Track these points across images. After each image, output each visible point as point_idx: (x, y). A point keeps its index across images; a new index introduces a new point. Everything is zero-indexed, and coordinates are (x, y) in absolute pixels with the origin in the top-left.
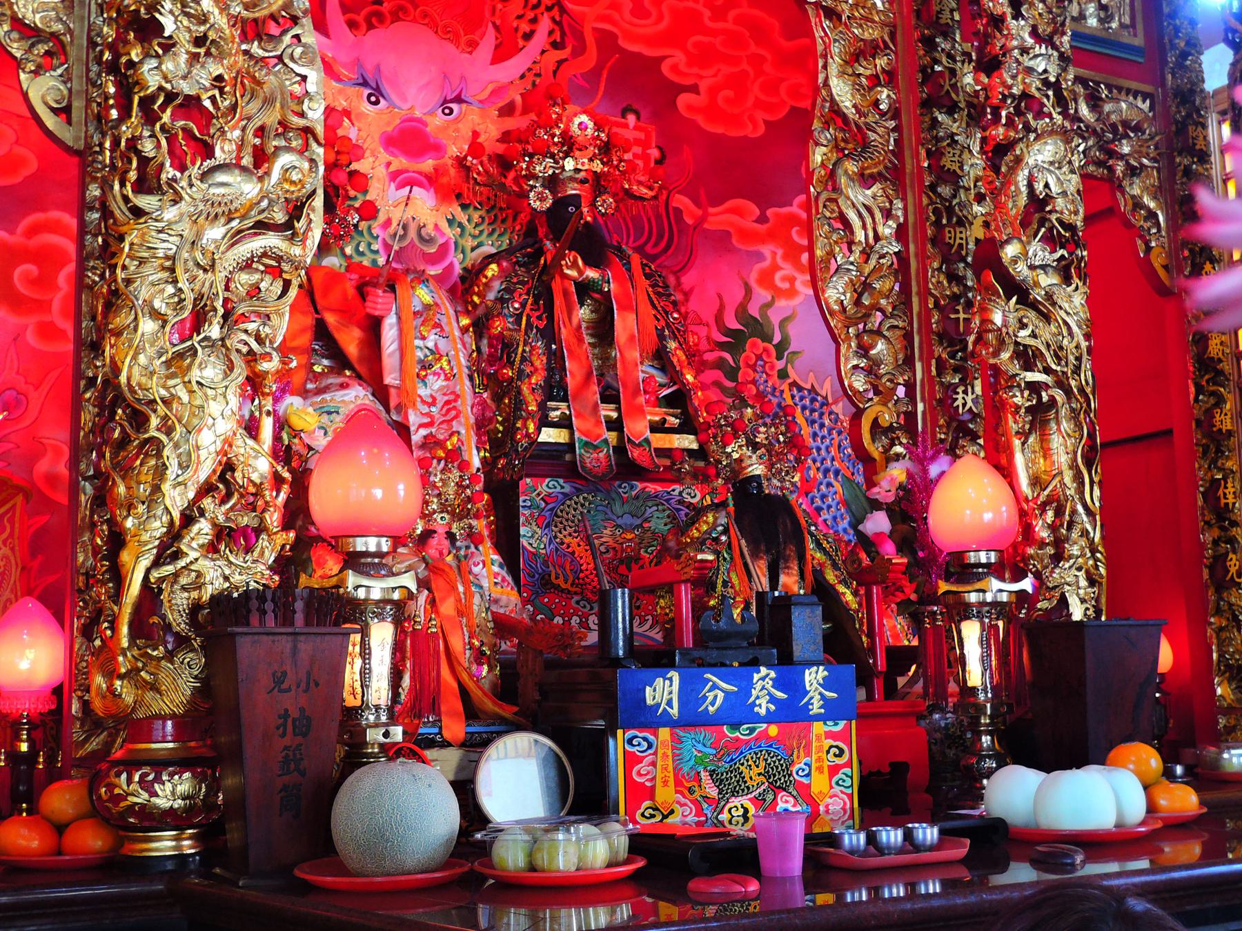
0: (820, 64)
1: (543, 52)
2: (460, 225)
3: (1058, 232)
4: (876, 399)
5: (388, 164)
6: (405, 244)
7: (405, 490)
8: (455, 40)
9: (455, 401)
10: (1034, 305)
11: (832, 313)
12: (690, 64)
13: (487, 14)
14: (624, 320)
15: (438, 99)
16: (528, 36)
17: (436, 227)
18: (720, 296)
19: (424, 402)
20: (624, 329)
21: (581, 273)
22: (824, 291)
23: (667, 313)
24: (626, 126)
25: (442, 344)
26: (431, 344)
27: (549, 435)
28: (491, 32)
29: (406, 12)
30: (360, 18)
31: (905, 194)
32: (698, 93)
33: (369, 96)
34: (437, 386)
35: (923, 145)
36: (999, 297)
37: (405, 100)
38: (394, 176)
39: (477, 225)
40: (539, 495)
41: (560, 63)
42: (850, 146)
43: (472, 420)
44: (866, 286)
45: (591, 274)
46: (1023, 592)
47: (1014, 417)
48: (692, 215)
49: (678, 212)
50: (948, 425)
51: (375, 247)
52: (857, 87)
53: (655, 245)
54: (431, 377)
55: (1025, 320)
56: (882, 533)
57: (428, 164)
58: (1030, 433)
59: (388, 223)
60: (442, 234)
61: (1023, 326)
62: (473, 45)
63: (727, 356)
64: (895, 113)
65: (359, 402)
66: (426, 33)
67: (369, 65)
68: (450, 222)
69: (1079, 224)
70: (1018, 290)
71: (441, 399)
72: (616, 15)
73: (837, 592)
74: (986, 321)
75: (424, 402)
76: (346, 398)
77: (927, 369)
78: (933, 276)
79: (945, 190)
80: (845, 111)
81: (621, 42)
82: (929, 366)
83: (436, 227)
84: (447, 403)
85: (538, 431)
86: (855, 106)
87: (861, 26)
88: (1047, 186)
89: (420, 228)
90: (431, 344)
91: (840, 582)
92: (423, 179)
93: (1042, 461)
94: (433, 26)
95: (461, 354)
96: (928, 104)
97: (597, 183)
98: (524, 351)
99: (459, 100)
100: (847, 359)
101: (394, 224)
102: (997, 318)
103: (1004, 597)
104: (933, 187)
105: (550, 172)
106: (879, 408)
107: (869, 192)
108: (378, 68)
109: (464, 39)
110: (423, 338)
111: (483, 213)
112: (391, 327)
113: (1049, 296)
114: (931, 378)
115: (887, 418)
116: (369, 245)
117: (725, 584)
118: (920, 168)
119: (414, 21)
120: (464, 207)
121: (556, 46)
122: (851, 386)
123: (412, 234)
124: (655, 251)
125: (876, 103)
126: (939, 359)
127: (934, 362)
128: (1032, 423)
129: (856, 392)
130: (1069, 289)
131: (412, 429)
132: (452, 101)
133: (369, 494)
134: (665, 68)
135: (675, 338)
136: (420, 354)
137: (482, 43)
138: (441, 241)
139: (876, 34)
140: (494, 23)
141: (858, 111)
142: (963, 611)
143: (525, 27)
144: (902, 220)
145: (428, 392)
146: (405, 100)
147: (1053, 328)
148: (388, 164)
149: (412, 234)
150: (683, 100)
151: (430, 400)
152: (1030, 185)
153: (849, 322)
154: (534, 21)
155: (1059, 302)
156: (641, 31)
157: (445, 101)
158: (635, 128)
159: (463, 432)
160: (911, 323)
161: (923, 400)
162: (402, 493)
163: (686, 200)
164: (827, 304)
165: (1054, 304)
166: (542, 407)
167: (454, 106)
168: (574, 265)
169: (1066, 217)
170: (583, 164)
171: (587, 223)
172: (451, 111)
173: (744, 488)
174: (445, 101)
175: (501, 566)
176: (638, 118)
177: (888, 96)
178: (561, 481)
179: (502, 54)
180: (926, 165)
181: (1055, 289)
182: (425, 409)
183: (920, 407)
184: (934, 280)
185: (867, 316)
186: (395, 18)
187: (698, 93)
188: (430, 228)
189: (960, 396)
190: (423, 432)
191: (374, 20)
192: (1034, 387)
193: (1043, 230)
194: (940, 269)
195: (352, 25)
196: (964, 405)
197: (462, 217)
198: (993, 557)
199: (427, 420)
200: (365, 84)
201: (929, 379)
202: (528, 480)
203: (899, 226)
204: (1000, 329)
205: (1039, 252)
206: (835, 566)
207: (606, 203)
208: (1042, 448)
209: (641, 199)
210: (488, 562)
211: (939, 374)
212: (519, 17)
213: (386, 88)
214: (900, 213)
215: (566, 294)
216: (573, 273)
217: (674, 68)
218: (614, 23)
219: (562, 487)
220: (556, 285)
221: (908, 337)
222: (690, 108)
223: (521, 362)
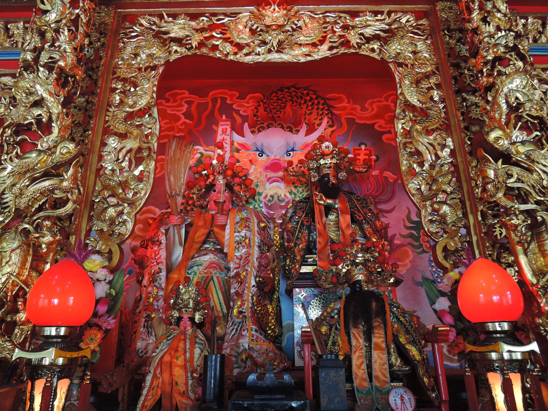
0: (398, 86)
1: (325, 129)
2: (294, 194)
3: (531, 122)
4: (445, 236)
5: (266, 176)
6: (272, 203)
7: (73, 300)
8: (291, 131)
9: (249, 256)
10: (517, 164)
11: (413, 195)
12: (386, 124)
13: (303, 120)
14: (344, 218)
15: (285, 151)
16: (319, 125)
17: (285, 195)
18: (408, 208)
19: (237, 258)
20: (345, 222)
21: (325, 202)
22: (407, 185)
23: (366, 214)
24: (361, 149)
25: (248, 234)
26: (243, 234)
27: (305, 269)
28: (305, 126)
29: (272, 125)
30: (256, 130)
31: (452, 135)
32: (391, 133)
33: (259, 154)
34: (244, 251)
35: (458, 110)
36: (491, 162)
37: (272, 153)
38: (268, 180)
39: (301, 193)
40: (302, 295)
41: (333, 132)
42: (419, 118)
43: (256, 264)
44: (435, 180)
45: (329, 201)
46: (533, 352)
47: (514, 233)
48: (392, 178)
49: (386, 178)
50: (493, 246)
51: (261, 205)
52: (419, 92)
53: (185, 94)
54: (241, 248)
55: (509, 172)
56: (443, 310)
57: (281, 174)
58: (531, 241)
59: (266, 196)
60: (288, 198)
61: (510, 176)
62: (298, 131)
63: (414, 232)
64: (443, 100)
65: (211, 260)
66: (279, 130)
67: (259, 144)
68: (290, 193)
69: (545, 115)
70: (506, 158)
71: (244, 256)
72: (354, 112)
73: (407, 349)
74: (486, 178)
75: (237, 258)
76: (205, 259)
77: (476, 218)
78: (472, 170)
79: (475, 128)
80: (414, 104)
81: (357, 121)
82: (477, 216)
83: (285, 195)
84: (246, 258)
85: (300, 268)
86: (418, 100)
87: (419, 67)
88: (517, 98)
89: (278, 197)
90: (243, 234)
91: (409, 343)
92: (280, 180)
93: (542, 259)
94: (282, 127)
95: (256, 237)
96: (458, 92)
97: (337, 168)
98: (298, 235)
99: (293, 150)
100: (425, 217)
101: (269, 196)
102: (491, 174)
103: (519, 356)
104: (467, 128)
105: (315, 166)
106: (447, 240)
107: (431, 137)
108: (262, 144)
109: (294, 130)
110: (239, 232)
111: (303, 188)
112: (228, 229)
113: (528, 157)
114: (479, 222)
115: (452, 245)
116: (259, 204)
117: (334, 343)
118: (459, 121)
119: (276, 127)
120: (295, 187)
121: (331, 126)
122: (428, 230)
123: (276, 199)
124: (377, 194)
125: (432, 98)
126: (482, 211)
127: (479, 213)
128: (532, 236)
129: (432, 233)
130: (543, 152)
131: (232, 270)
132: (290, 151)
133: (50, 302)
134: (376, 127)
135: (368, 223)
136: (237, 239)
137: (301, 130)
138: (287, 200)
139: (429, 69)
140: (306, 123)
141: (421, 102)
142: (490, 366)
143: (317, 122)
144: (452, 147)
145: (240, 254)
146: (272, 153)
147: (535, 176)
148: (266, 176)
149: (276, 199)
150: (384, 137)
151: (240, 257)
152: (507, 102)
153: (424, 199)
154: (321, 119)
155: (536, 159)
156: (366, 115)
157: (288, 151)
158: (365, 150)
159: (249, 270)
160: (463, 196)
161: (476, 234)
162: (72, 301)
163: (389, 173)
164: (410, 191)
165: (533, 161)
166: (303, 257)
167: (291, 153)
168: (321, 199)
169: (534, 113)
170: (328, 161)
171: (333, 183)
172: (290, 154)
173: (355, 285)
174: (288, 151)
175: (256, 331)
176: (366, 145)
177: (438, 94)
178: (313, 289)
179: (308, 133)
180: (461, 119)
181: (531, 152)
182: (238, 261)
183: (475, 238)
184: (473, 172)
185: (436, 195)
186: (268, 127)
187: (391, 133)
188: (283, 196)
189: (498, 229)
190: (235, 271)
191: (261, 129)
192: (530, 213)
193: (520, 123)
194: (476, 167)
195: (253, 132)
196: (501, 234)
197: (294, 190)
198: (506, 326)
199: (237, 266)
200: (258, 150)
201: (477, 223)
202: (297, 289)
203: (451, 150)
204: (494, 181)
205: (518, 135)
206: (407, 332)
207: (343, 175)
208: (540, 250)
209: (361, 172)
210: (250, 329)
211: (483, 219)
212: (315, 119)
213: (265, 150)
214: (451, 144)
215: (320, 211)
216: (322, 202)
217: (380, 126)
218: (353, 115)
219: (313, 292)
220: (316, 207)
221: (462, 202)
222: (388, 139)
223: (296, 240)
